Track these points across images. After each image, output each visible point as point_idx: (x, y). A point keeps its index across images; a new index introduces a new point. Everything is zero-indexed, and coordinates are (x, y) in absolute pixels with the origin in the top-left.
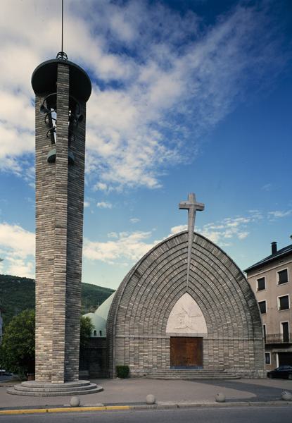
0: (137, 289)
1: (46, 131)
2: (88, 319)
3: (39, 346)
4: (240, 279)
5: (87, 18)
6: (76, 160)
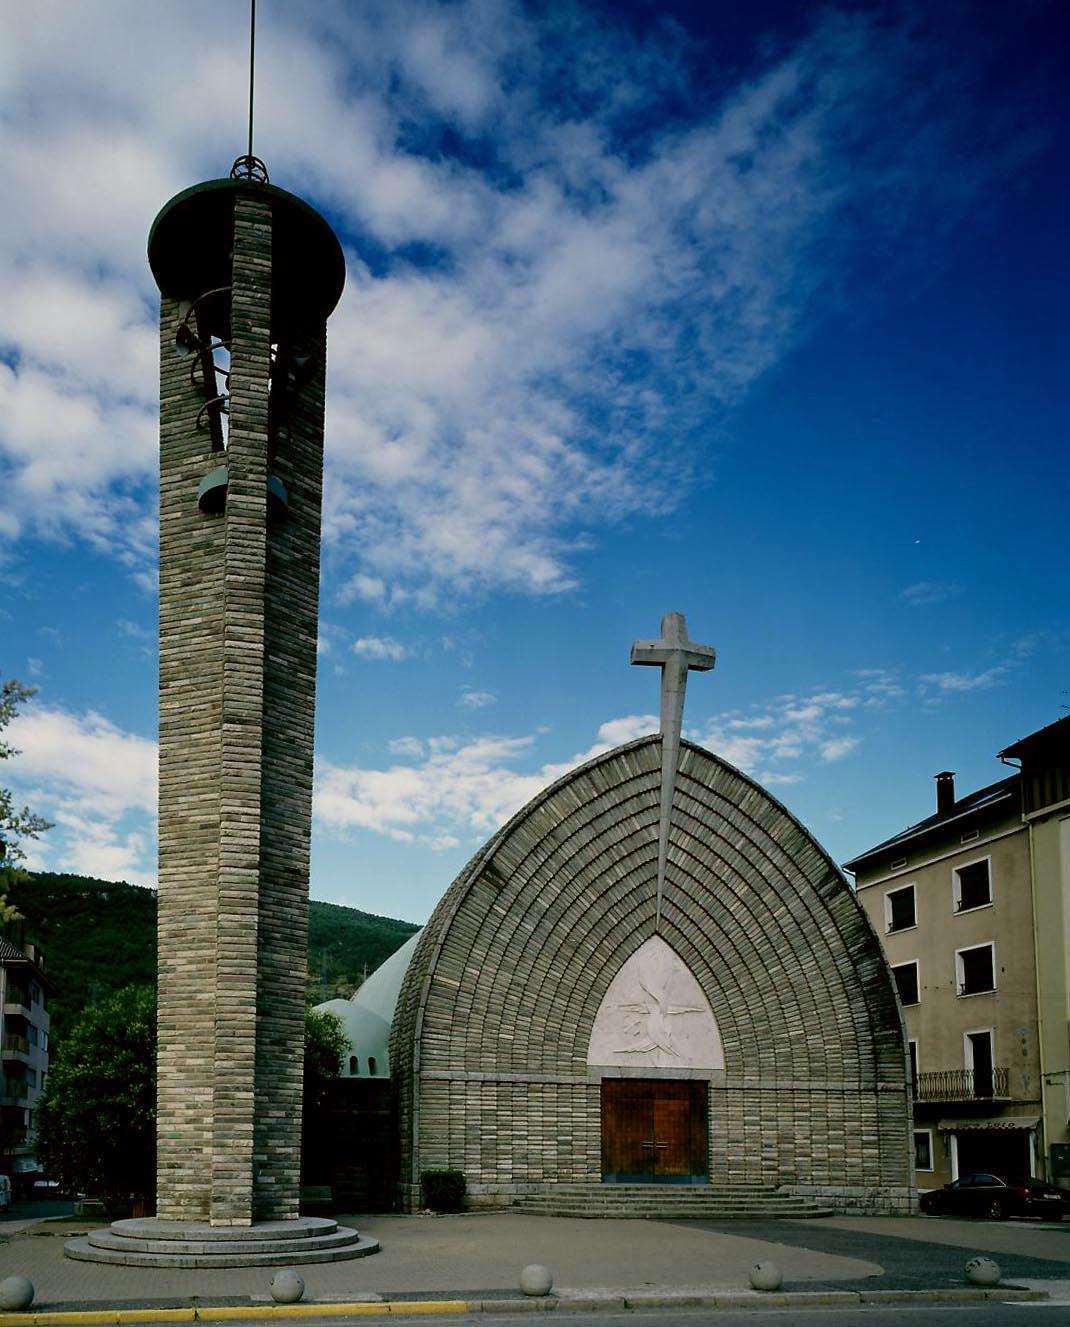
0: (494, 921)
1: (195, 411)
2: (330, 1021)
3: (171, 1105)
4: (833, 894)
5: (326, 38)
6: (292, 502)
